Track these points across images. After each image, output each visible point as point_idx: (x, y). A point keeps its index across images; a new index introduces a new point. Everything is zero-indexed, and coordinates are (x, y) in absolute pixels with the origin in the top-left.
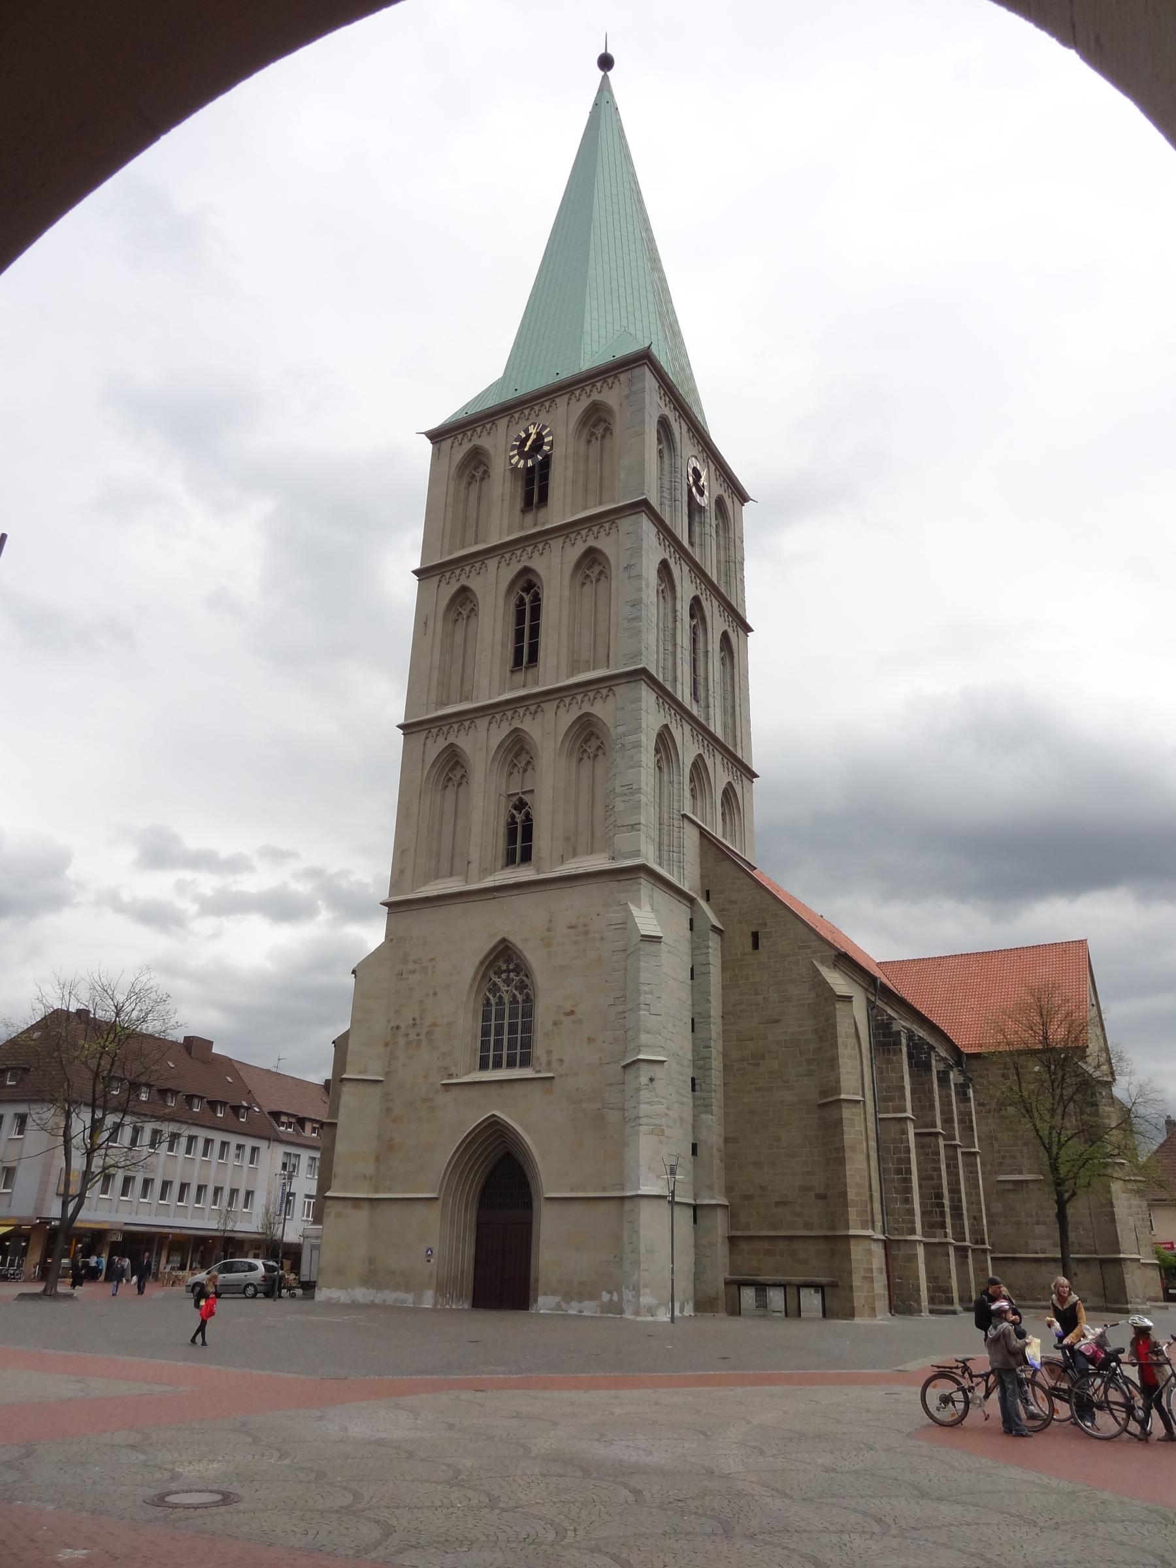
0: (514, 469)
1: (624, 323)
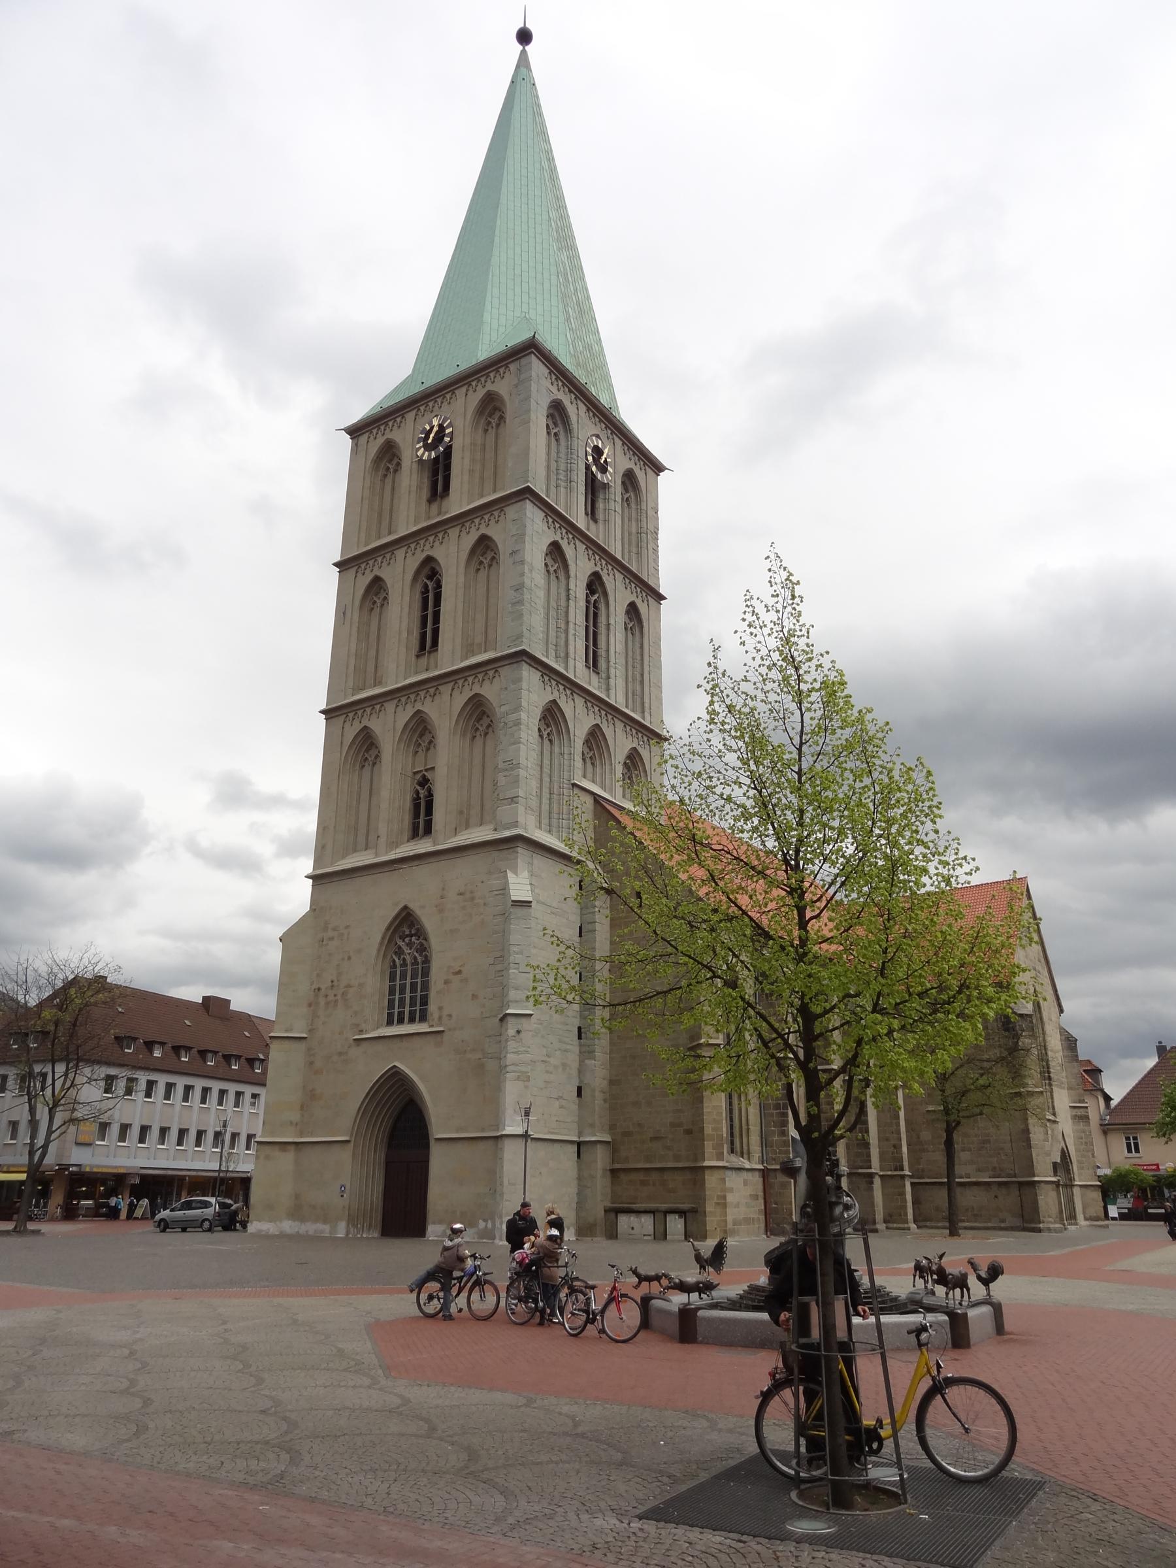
0: (420, 461)
1: (525, 308)
